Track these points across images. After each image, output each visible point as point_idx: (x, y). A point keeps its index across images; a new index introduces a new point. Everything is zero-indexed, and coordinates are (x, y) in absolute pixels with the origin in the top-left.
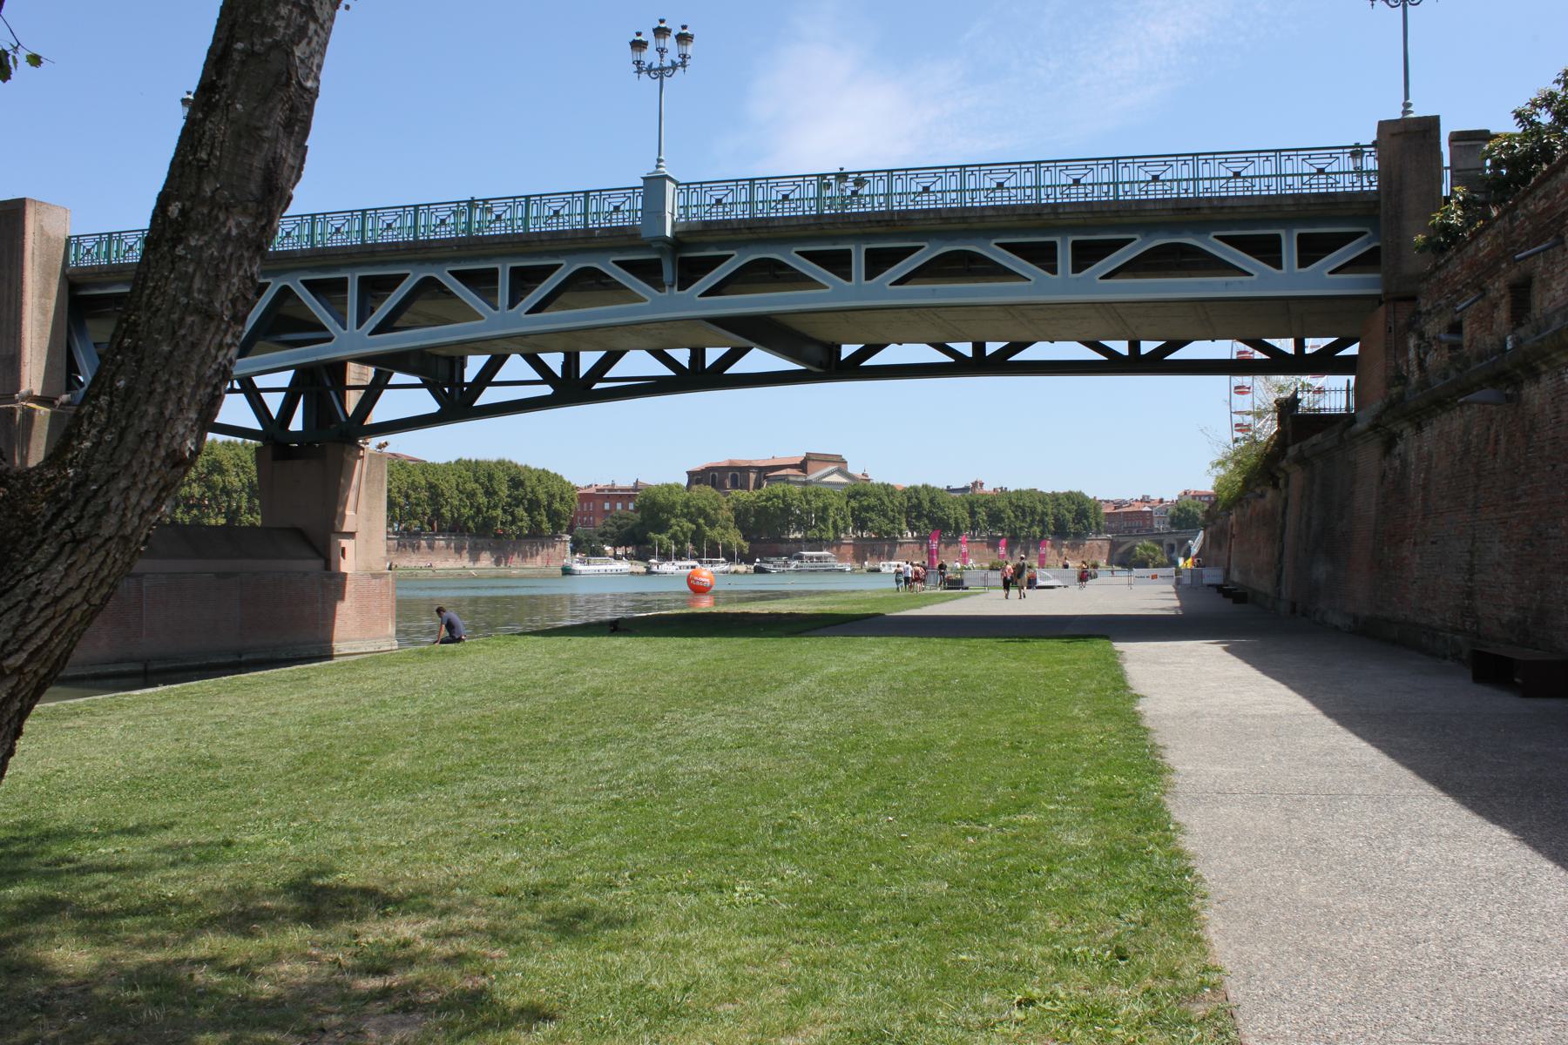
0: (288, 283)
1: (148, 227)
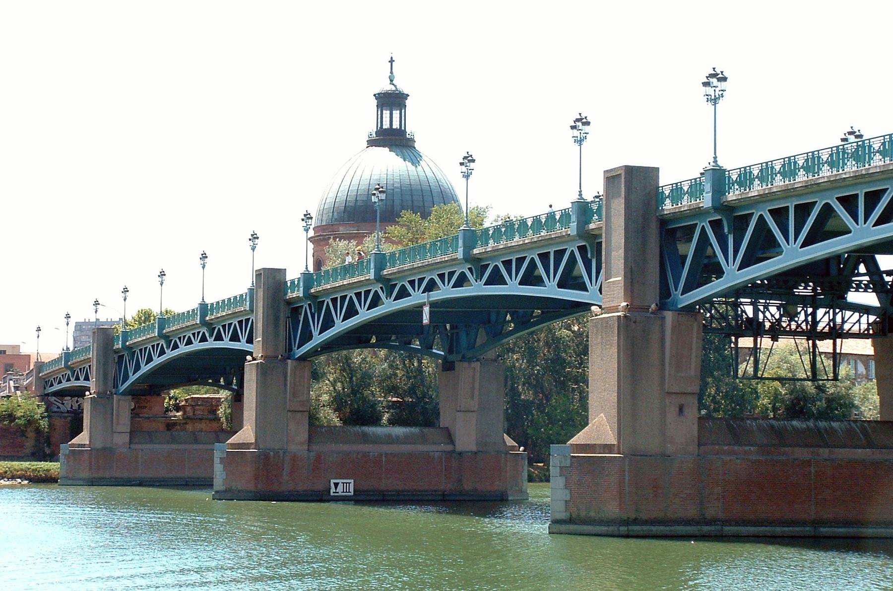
0: (404, 283)
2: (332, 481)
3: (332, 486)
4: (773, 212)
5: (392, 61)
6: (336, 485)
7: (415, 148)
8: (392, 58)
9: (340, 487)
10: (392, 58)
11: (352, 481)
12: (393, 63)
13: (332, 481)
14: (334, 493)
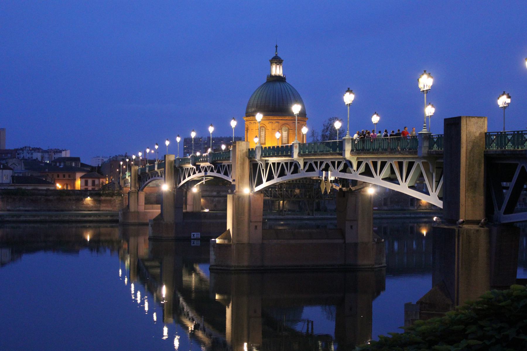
1: (443, 134)
2: (192, 234)
3: (192, 236)
4: (373, 162)
5: (276, 47)
6: (194, 235)
7: (286, 82)
8: (276, 45)
9: (195, 236)
10: (276, 45)
11: (199, 233)
12: (277, 48)
13: (192, 234)
14: (193, 237)
